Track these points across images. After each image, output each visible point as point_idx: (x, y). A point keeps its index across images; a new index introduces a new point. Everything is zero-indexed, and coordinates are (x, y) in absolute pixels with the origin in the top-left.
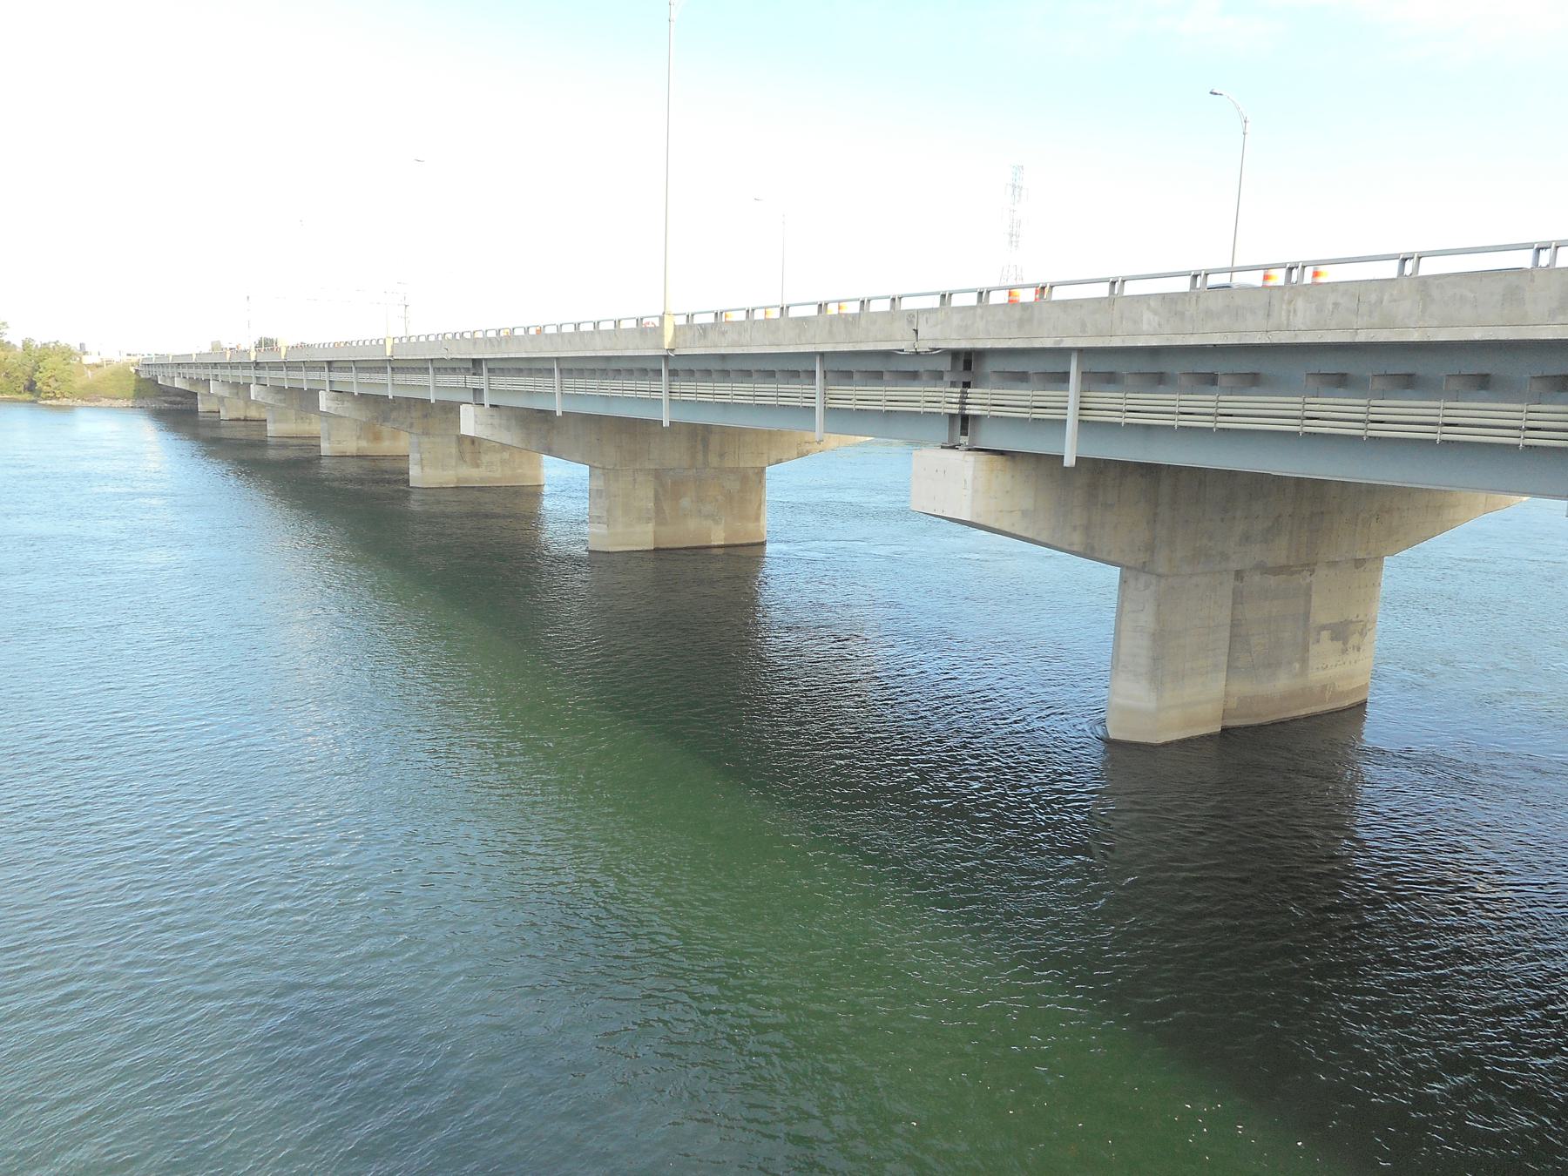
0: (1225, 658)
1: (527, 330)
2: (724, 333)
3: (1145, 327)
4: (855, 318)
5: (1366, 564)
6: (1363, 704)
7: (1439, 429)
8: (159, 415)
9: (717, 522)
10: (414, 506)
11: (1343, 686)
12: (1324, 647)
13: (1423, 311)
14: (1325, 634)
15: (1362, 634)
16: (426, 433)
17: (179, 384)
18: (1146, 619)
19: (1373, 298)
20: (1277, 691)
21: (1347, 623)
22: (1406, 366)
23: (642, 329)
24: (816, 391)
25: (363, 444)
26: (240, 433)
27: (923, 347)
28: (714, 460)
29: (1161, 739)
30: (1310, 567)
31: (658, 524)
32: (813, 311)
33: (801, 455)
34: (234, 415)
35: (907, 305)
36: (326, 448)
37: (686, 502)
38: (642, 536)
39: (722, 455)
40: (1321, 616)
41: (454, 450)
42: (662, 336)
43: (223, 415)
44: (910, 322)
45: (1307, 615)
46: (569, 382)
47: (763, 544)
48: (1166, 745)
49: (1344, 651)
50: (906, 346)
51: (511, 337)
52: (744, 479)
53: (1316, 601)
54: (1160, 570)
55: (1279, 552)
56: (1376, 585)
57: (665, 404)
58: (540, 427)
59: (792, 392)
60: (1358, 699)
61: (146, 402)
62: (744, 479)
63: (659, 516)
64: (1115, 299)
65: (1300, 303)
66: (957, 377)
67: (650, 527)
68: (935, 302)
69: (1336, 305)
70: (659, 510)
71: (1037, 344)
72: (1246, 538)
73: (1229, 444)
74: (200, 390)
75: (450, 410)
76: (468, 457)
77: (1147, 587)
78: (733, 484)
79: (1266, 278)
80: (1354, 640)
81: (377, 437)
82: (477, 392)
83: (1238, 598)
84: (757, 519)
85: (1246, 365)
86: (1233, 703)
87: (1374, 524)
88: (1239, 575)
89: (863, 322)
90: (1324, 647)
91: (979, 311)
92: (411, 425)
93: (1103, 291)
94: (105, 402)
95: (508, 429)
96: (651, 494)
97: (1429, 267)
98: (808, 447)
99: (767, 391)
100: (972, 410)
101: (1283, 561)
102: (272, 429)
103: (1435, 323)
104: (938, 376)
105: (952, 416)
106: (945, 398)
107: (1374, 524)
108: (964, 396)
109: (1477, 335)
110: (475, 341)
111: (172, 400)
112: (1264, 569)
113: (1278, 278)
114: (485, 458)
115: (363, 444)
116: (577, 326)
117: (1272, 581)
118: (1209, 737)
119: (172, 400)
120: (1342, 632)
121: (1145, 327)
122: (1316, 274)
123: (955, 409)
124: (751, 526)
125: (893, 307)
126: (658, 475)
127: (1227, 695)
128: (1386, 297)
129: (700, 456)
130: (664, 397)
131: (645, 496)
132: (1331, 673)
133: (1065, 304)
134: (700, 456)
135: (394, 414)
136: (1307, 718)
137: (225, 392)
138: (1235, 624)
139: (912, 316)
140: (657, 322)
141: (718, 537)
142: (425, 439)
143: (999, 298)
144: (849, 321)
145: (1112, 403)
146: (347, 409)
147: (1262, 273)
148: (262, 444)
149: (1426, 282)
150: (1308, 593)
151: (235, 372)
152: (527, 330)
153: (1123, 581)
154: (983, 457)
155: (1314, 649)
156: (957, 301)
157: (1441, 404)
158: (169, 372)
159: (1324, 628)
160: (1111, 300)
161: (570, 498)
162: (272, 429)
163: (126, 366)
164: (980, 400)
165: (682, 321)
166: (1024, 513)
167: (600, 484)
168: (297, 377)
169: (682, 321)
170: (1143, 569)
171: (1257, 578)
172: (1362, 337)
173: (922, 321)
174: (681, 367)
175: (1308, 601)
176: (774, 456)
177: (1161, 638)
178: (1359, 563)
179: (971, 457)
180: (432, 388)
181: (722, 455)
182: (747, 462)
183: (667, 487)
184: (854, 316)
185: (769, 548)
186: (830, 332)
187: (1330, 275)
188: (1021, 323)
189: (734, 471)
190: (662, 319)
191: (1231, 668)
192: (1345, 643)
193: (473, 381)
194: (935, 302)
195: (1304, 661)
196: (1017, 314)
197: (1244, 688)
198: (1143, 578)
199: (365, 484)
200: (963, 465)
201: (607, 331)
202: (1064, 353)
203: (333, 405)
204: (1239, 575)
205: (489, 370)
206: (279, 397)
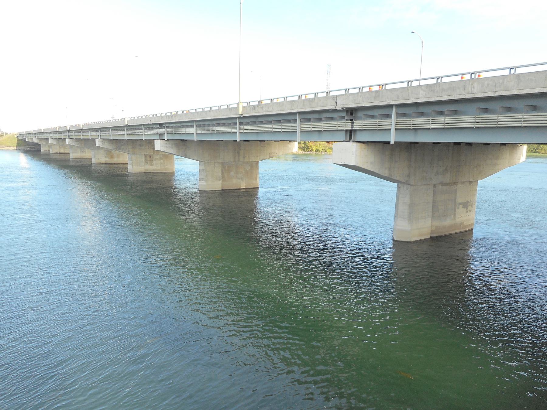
0: (431, 213)
1: (183, 112)
2: (262, 108)
3: (421, 96)
4: (313, 99)
5: (473, 183)
6: (472, 229)
7: (523, 122)
8: (26, 152)
9: (243, 181)
10: (130, 178)
11: (467, 223)
12: (461, 210)
13: (518, 85)
14: (461, 206)
15: (472, 206)
16: (134, 154)
17: (35, 140)
18: (407, 200)
19: (501, 81)
20: (447, 224)
21: (467, 202)
22: (508, 102)
23: (229, 109)
24: (297, 126)
25: (107, 159)
26: (58, 157)
27: (339, 107)
28: (241, 159)
29: (412, 240)
30: (456, 183)
31: (223, 181)
32: (297, 98)
33: (271, 157)
34: (55, 151)
35: (332, 94)
36: (94, 161)
37: (232, 174)
38: (217, 185)
39: (244, 157)
40: (460, 200)
41: (143, 159)
42: (239, 110)
43: (51, 151)
44: (334, 99)
45: (455, 199)
46: (200, 129)
47: (258, 188)
48: (414, 242)
49: (467, 212)
50: (332, 108)
51: (177, 115)
52: (252, 166)
53: (458, 195)
54: (412, 183)
55: (447, 178)
56: (476, 190)
57: (238, 133)
58: (183, 146)
59: (288, 127)
60: (471, 228)
61: (21, 148)
62: (252, 166)
63: (223, 178)
64: (409, 88)
65: (476, 85)
66: (349, 117)
67: (220, 182)
68: (343, 92)
69: (488, 84)
70: (223, 176)
71: (381, 104)
72: (437, 173)
73: (436, 140)
74: (43, 143)
75: (151, 142)
76: (148, 162)
77: (407, 189)
78: (248, 167)
79: (462, 78)
80: (470, 208)
81: (112, 157)
82: (161, 135)
83: (435, 194)
84: (256, 179)
85: (453, 107)
86: (434, 229)
87: (475, 169)
88: (435, 185)
89: (316, 101)
90: (461, 210)
91: (360, 94)
92: (129, 151)
93: (405, 85)
94: (6, 148)
95: (172, 148)
96: (221, 171)
97: (519, 71)
98: (273, 155)
99: (278, 127)
100: (355, 128)
101: (448, 181)
102: (72, 155)
103: (522, 88)
104: (343, 118)
105: (347, 131)
106: (346, 125)
107: (475, 169)
108: (353, 123)
109: (537, 91)
110: (162, 117)
111: (31, 147)
112: (442, 184)
113: (467, 77)
114: (155, 162)
115: (107, 159)
116: (203, 109)
117: (445, 188)
118: (426, 240)
119: (31, 147)
120: (466, 205)
121: (421, 96)
122: (479, 76)
123: (349, 128)
124: (254, 182)
125: (327, 95)
126: (223, 164)
127: (432, 225)
128: (505, 81)
129: (237, 158)
130: (238, 132)
131: (218, 171)
132: (461, 219)
133: (391, 90)
134: (237, 158)
135: (123, 147)
136: (456, 233)
137: (54, 142)
138: (434, 202)
139: (334, 97)
140: (235, 106)
141: (243, 185)
142: (133, 156)
143: (366, 90)
144: (311, 101)
145: (406, 122)
146: (106, 145)
147: (460, 76)
148: (68, 160)
149: (519, 75)
150: (455, 192)
151: (60, 135)
152: (183, 112)
153: (398, 188)
154: (358, 144)
155: (458, 211)
156: (351, 91)
157: (523, 115)
158: (31, 136)
159: (460, 204)
160: (408, 88)
161: (189, 173)
162: (72, 155)
163: (13, 135)
164: (358, 124)
165: (246, 104)
166: (371, 163)
167: (203, 167)
168: (85, 137)
169: (246, 104)
170: (407, 183)
171: (440, 187)
172: (497, 94)
173: (338, 98)
174: (244, 120)
175: (456, 195)
176: (262, 157)
177: (412, 206)
178: (471, 182)
179: (355, 144)
180: (143, 135)
181: (244, 157)
182: (253, 160)
183: (226, 168)
184: (312, 99)
185: (260, 189)
186: (304, 105)
187: (483, 75)
188: (375, 97)
189: (248, 163)
190: (238, 104)
191: (433, 217)
192: (467, 209)
193: (160, 131)
194: (343, 92)
195: (455, 215)
196: (374, 94)
197: (437, 223)
198: (406, 186)
199: (115, 170)
200: (352, 147)
201: (216, 110)
202: (390, 106)
203: (100, 143)
204: (435, 185)
205: (167, 127)
206: (76, 143)
